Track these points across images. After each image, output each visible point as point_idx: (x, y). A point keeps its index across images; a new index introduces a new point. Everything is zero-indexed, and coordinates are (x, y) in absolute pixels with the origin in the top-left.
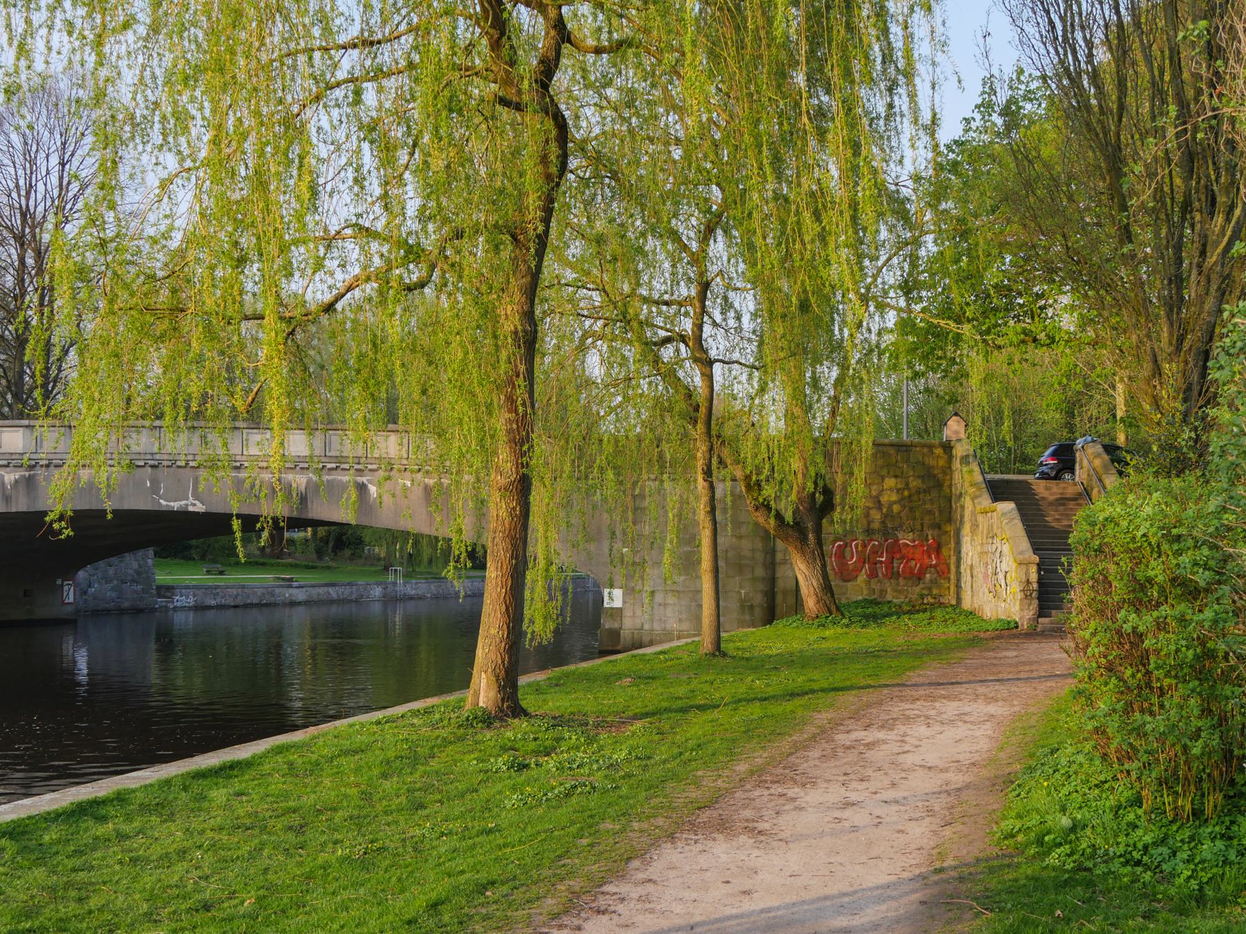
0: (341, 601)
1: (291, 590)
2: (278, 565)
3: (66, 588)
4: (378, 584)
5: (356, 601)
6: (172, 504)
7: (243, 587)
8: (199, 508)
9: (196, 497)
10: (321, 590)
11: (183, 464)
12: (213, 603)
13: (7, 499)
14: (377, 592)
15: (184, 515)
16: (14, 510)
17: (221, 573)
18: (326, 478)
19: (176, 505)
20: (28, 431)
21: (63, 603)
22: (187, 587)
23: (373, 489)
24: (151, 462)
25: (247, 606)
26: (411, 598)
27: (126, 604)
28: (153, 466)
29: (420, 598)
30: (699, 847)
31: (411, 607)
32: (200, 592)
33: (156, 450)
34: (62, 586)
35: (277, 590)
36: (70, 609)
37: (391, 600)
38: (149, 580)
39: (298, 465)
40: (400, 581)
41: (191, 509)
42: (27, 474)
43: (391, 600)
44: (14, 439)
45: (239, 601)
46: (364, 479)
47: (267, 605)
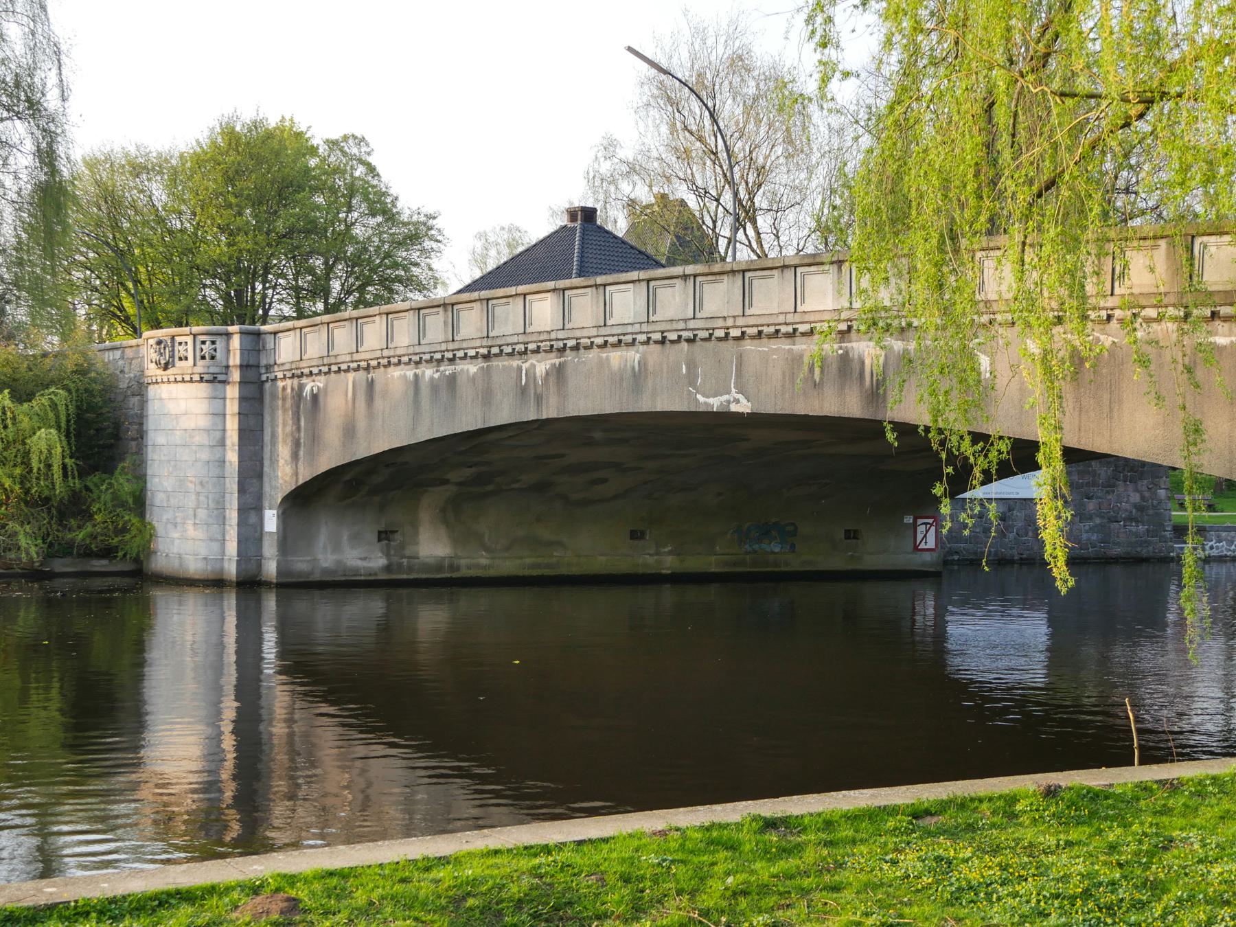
3: (921, 529)
6: (711, 400)
8: (743, 406)
11: (722, 335)
15: (725, 419)
16: (544, 417)
19: (715, 403)
21: (916, 548)
24: (685, 334)
27: (1117, 551)
34: (915, 526)
36: (927, 557)
41: (734, 408)
42: (557, 361)
44: (1233, 339)
47: (1140, 560)
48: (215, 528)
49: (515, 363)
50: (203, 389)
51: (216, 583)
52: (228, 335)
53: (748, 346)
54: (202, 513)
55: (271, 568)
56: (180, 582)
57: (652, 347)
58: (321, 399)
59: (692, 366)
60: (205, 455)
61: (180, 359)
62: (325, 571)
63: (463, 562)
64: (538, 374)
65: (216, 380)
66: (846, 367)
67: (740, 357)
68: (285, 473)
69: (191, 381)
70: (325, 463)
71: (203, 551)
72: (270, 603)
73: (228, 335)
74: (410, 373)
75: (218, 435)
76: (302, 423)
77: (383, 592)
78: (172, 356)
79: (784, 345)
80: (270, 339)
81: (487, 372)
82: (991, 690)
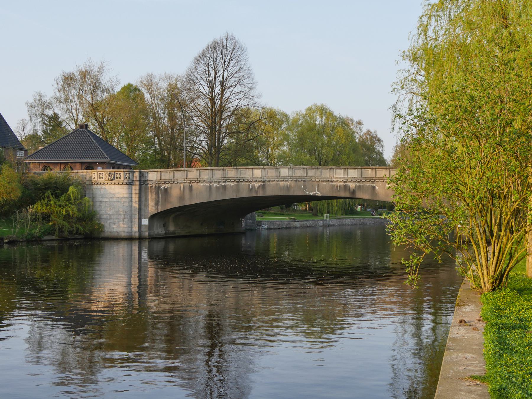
0: (310, 227)
1: (296, 223)
2: (270, 213)
4: (321, 220)
5: (315, 227)
7: (281, 221)
9: (318, 191)
10: (304, 223)
12: (273, 227)
13: (256, 192)
14: (321, 223)
17: (262, 216)
18: (361, 184)
19: (312, 194)
20: (263, 170)
22: (265, 222)
23: (377, 188)
25: (282, 228)
26: (331, 226)
28: (304, 181)
29: (334, 226)
30: (527, 262)
31: (332, 228)
32: (269, 223)
33: (305, 175)
35: (291, 223)
37: (326, 226)
38: (254, 219)
39: (354, 180)
40: (328, 219)
41: (317, 195)
43: (326, 226)
45: (280, 227)
46: (374, 185)
48: (130, 224)
49: (248, 183)
50: (126, 187)
51: (130, 239)
52: (134, 172)
53: (320, 183)
54: (126, 220)
55: (147, 234)
56: (117, 239)
57: (293, 182)
58: (169, 190)
59: (305, 186)
60: (127, 204)
61: (117, 178)
62: (156, 235)
63: (176, 232)
64: (99, 175)
65: (130, 184)
66: (346, 188)
67: (318, 185)
68: (151, 208)
69: (122, 184)
70: (169, 207)
71: (126, 230)
72: (146, 243)
73: (134, 172)
74: (208, 185)
75: (130, 199)
76: (160, 196)
77: (126, 242)
78: (114, 177)
79: (330, 183)
80: (144, 173)
81: (237, 186)
82: (188, 268)
